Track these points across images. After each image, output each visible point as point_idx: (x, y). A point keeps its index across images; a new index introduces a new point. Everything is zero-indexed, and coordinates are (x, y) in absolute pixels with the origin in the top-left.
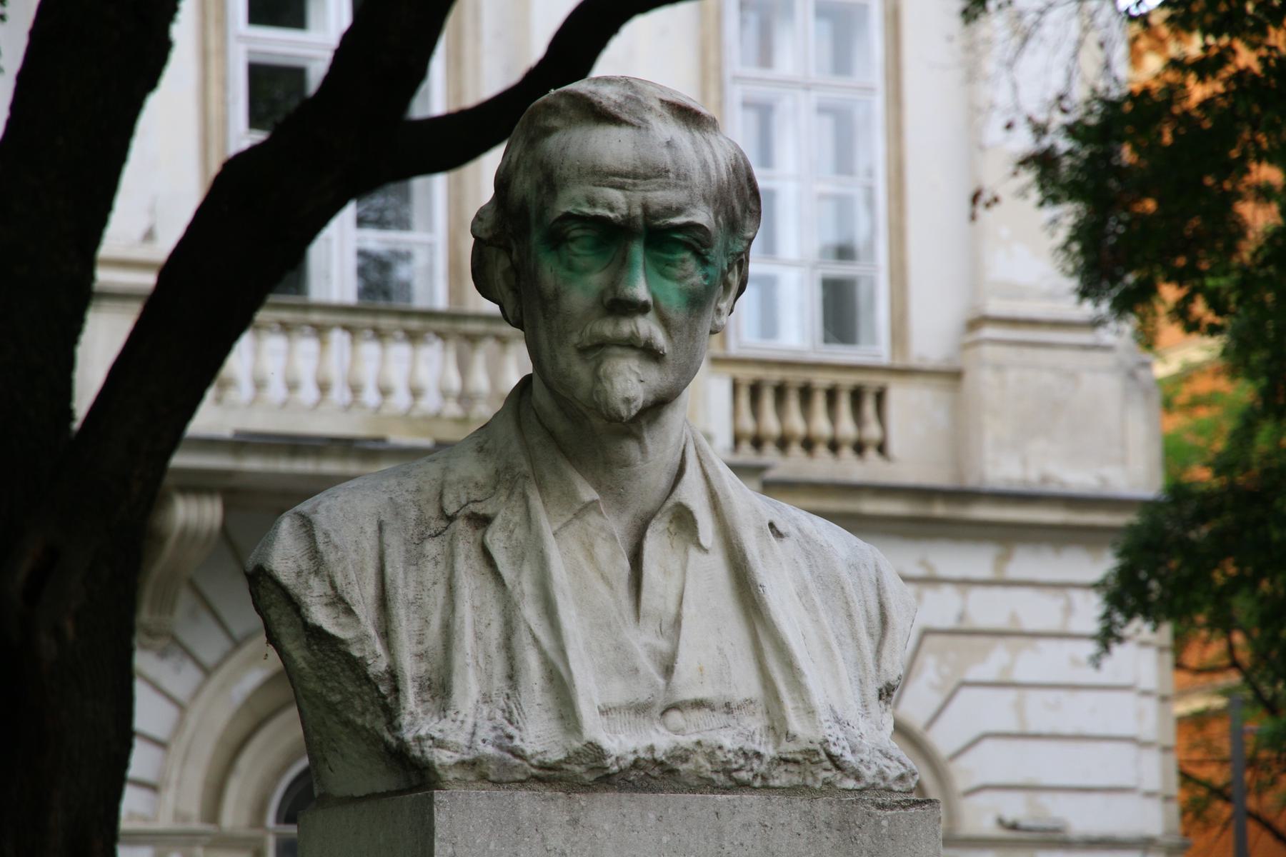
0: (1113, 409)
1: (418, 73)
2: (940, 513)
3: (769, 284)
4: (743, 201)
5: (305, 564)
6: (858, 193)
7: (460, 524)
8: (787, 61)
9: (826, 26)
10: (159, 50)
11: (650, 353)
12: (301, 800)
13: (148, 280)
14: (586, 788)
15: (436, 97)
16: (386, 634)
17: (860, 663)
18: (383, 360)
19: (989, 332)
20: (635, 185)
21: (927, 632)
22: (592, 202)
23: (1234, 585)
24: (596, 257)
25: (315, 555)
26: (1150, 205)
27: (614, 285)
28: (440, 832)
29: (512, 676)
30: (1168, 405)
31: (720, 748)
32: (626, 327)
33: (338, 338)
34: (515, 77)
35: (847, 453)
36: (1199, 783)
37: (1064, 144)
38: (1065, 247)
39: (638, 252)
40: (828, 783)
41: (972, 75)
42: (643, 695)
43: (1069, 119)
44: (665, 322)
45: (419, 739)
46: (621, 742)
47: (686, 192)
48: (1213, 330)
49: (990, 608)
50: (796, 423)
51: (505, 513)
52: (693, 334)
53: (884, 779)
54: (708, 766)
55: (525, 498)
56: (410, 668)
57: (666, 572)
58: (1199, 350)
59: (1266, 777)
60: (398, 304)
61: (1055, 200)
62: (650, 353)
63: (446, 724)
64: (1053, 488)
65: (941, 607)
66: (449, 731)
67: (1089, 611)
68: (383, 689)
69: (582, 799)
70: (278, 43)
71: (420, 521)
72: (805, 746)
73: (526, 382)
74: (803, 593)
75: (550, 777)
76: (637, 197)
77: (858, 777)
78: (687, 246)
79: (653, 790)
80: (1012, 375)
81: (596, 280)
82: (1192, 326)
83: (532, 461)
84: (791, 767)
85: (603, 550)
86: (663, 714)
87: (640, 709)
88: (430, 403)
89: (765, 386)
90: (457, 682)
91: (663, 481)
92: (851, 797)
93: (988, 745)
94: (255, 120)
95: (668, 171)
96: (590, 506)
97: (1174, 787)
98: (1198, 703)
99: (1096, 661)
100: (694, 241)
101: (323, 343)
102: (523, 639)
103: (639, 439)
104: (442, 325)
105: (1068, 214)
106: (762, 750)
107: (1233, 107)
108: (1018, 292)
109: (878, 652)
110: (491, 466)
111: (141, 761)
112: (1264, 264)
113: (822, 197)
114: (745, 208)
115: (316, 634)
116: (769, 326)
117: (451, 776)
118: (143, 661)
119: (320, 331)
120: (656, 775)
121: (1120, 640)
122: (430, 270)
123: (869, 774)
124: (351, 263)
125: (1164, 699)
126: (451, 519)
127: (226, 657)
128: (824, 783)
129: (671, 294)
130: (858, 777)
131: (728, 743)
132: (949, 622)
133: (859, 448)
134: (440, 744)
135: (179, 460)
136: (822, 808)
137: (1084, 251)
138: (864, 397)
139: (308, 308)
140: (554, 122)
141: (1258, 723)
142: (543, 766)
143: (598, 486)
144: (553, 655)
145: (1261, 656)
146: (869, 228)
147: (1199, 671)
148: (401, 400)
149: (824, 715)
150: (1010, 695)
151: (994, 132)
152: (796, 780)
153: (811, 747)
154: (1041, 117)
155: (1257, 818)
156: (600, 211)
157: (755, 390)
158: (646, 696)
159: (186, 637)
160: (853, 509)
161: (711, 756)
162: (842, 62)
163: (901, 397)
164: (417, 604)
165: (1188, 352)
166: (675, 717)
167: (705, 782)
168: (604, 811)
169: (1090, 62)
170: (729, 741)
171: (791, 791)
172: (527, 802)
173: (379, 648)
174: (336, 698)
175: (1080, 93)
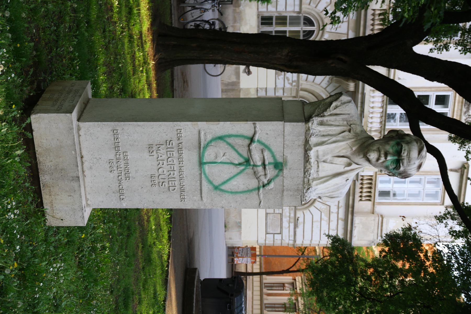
0: (367, 239)
1: (428, 123)
2: (350, 210)
3: (389, 182)
4: (405, 175)
5: (343, 102)
6: (405, 198)
7: (349, 127)
8: (428, 186)
9: (434, 193)
10: (432, 80)
11: (378, 160)
12: (303, 103)
13: (392, 77)
14: (305, 148)
15: (423, 127)
16: (331, 115)
17: (325, 193)
18: (377, 117)
19: (380, 219)
21: (330, 206)
22: (404, 150)
23: (337, 257)
24: (394, 150)
25: (344, 103)
26: (402, 246)
27: (390, 153)
28: (298, 123)
29: (323, 136)
30: (368, 248)
32: (383, 155)
33: (381, 110)
34: (426, 140)
35: (360, 194)
36: (305, 250)
37: (413, 232)
38: (395, 232)
39: (396, 158)
40: (305, 187)
41: (425, 217)
42: (320, 157)
43: (417, 233)
44: (383, 162)
45: (313, 120)
46: (312, 154)
48: (380, 256)
49: (334, 217)
50: (365, 186)
51: (351, 135)
52: (381, 167)
55: (353, 138)
56: (325, 119)
57: (340, 162)
58: (377, 254)
59: (305, 261)
60: (386, 121)
61: (403, 230)
62: (378, 160)
63: (316, 125)
64: (354, 228)
65: (334, 209)
66: (314, 125)
67: (333, 233)
68: (322, 114)
69: (303, 147)
70: (432, 101)
71: (350, 121)
73: (373, 139)
74: (337, 184)
75: (307, 142)
76: (405, 158)
77: (306, 192)
78: (396, 166)
80: (373, 222)
81: (391, 151)
82: (381, 252)
83: (360, 139)
85: (344, 151)
87: (318, 157)
88: (370, 125)
89: (371, 181)
90: (323, 126)
91: (356, 161)
94: (418, 96)
97: (304, 246)
98: (318, 251)
99: (325, 234)
100: (397, 167)
101: (380, 107)
102: (329, 138)
103: (363, 157)
104: (383, 127)
105: (401, 232)
107: (419, 261)
108: (387, 224)
109: (327, 196)
110: (359, 133)
111: (311, 77)
112: (392, 265)
113: (404, 191)
114: (403, 176)
115: (331, 103)
116: (382, 182)
118: (328, 77)
119: (382, 107)
120: (307, 159)
121: (328, 238)
122: (393, 126)
123: (306, 194)
124: (394, 112)
125: (318, 245)
126: (350, 126)
127: (328, 92)
129: (388, 163)
130: (306, 192)
131: (312, 171)
132: (331, 210)
133: (361, 196)
134: (312, 124)
135: (361, 83)
136: (301, 186)
137: (394, 235)
138: (369, 198)
139: (386, 105)
140: (419, 144)
141: (314, 260)
142: (308, 141)
143: (355, 150)
144: (327, 142)
145: (326, 261)
146: (399, 199)
147: (323, 251)
148: (370, 120)
149: (316, 187)
150: (320, 220)
151: (415, 220)
152: (306, 182)
154: (418, 228)
155: (299, 259)
156: (403, 151)
157: (371, 179)
159: (331, 85)
160: (350, 195)
162: (428, 195)
163: (370, 203)
164: (336, 120)
165: (376, 252)
166: (316, 163)
168: (301, 151)
169: (428, 237)
170: (312, 171)
171: (304, 181)
172: (302, 138)
173: (329, 114)
174: (320, 107)
175: (422, 235)
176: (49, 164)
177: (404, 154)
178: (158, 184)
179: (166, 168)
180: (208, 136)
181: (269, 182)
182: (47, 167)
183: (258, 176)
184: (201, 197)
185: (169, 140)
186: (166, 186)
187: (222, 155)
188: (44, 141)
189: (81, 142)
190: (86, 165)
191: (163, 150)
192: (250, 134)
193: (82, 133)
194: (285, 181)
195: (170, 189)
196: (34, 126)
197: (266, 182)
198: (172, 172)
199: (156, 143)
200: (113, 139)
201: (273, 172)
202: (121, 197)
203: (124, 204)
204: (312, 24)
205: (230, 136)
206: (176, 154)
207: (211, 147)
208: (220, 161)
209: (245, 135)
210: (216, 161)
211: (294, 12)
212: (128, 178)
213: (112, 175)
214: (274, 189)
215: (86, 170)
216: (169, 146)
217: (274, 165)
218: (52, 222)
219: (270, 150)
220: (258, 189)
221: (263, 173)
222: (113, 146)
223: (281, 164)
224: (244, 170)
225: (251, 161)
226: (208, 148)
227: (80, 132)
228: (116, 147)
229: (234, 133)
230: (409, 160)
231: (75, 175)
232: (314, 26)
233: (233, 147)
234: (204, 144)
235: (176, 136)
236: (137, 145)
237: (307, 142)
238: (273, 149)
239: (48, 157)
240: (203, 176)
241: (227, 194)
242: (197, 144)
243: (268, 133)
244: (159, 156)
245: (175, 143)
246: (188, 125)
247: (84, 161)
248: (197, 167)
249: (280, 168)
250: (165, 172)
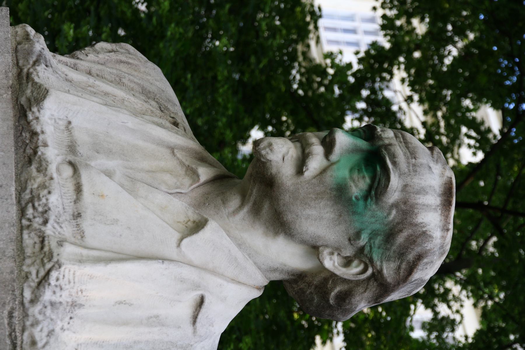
14: (16, 100)
20: (401, 142)
31: (49, 193)
40: (27, 277)
42: (82, 150)
44: (324, 171)
46: (49, 117)
47: (406, 170)
53: (32, 325)
54: (35, 186)
69: (8, 95)
72: (55, 252)
76: (394, 141)
78: (373, 179)
84: (38, 246)
87: (72, 148)
92: (17, 293)
95: (415, 158)
106: (49, 225)
123: (35, 310)
128: (27, 273)
129: (342, 172)
130: (33, 301)
152: (29, 251)
153: (55, 254)
158: (81, 151)
161: (43, 186)
166: (68, 171)
167: (24, 186)
171: (21, 250)
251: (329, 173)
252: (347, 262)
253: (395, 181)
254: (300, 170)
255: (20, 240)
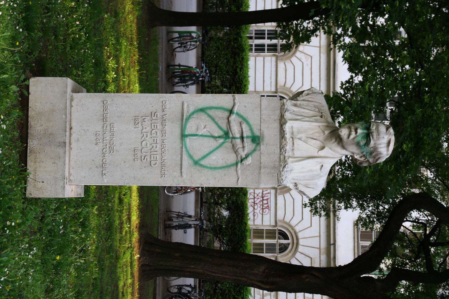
7: (321, 114)
14: (280, 122)
16: (303, 100)
32: (353, 130)
42: (295, 134)
44: (354, 138)
46: (287, 127)
56: (298, 102)
62: (349, 135)
69: (278, 122)
71: (321, 109)
75: (282, 116)
76: (374, 131)
78: (367, 141)
79: (280, 134)
85: (317, 135)
86: (292, 137)
87: (292, 133)
93: (293, 82)
96: (324, 132)
102: (303, 117)
117: (282, 101)
123: (283, 173)
129: (359, 139)
142: (283, 115)
152: (282, 160)
161: (285, 144)
166: (291, 139)
168: (276, 125)
172: (278, 112)
176: (39, 128)
177: (373, 128)
178: (140, 158)
179: (149, 140)
180: (191, 108)
181: (247, 156)
182: (36, 131)
183: (237, 149)
184: (181, 173)
185: (155, 112)
186: (148, 160)
187: (203, 127)
188: (38, 104)
189: (72, 113)
190: (74, 136)
191: (147, 122)
192: (229, 106)
193: (74, 104)
194: (262, 157)
195: (152, 164)
196: (31, 89)
197: (244, 156)
198: (154, 145)
199: (142, 115)
200: (102, 110)
201: (251, 146)
202: (103, 171)
203: (105, 180)
204: (286, 238)
205: (211, 108)
206: (159, 127)
207: (193, 119)
208: (200, 134)
209: (225, 107)
210: (197, 133)
211: (270, 226)
212: (111, 150)
213: (97, 148)
214: (252, 165)
215: (73, 142)
216: (154, 118)
217: (251, 139)
218: (33, 191)
219: (248, 123)
220: (237, 164)
221: (241, 146)
222: (102, 118)
223: (259, 138)
224: (223, 143)
225: (230, 133)
226: (190, 120)
227: (72, 103)
228: (104, 119)
229: (214, 105)
230: (378, 134)
231: (62, 141)
232: (288, 239)
233: (213, 119)
234: (187, 116)
235: (161, 108)
236: (124, 117)
237: (282, 116)
238: (251, 122)
239: (39, 121)
240: (184, 149)
241: (206, 170)
242: (179, 116)
243: (246, 105)
244: (144, 128)
245: (159, 114)
246: (172, 97)
247: (72, 133)
248: (179, 140)
249: (257, 142)
250: (148, 145)
251: (356, 139)
252: (361, 157)
253: (372, 142)
254: (348, 138)
255: (280, 157)
